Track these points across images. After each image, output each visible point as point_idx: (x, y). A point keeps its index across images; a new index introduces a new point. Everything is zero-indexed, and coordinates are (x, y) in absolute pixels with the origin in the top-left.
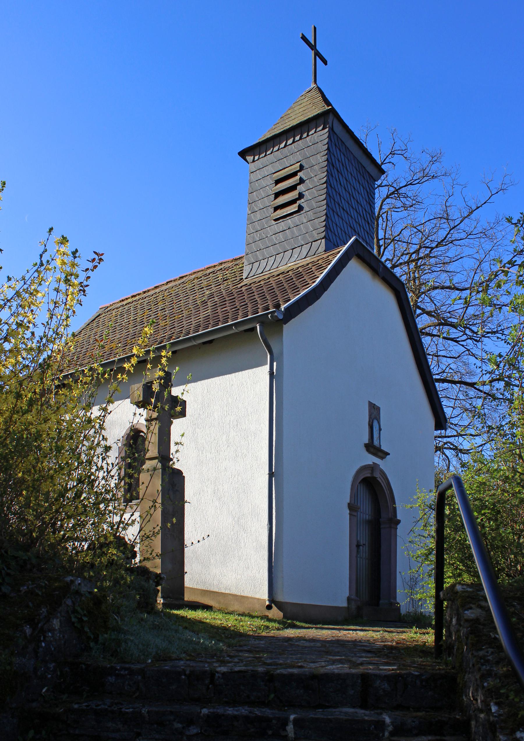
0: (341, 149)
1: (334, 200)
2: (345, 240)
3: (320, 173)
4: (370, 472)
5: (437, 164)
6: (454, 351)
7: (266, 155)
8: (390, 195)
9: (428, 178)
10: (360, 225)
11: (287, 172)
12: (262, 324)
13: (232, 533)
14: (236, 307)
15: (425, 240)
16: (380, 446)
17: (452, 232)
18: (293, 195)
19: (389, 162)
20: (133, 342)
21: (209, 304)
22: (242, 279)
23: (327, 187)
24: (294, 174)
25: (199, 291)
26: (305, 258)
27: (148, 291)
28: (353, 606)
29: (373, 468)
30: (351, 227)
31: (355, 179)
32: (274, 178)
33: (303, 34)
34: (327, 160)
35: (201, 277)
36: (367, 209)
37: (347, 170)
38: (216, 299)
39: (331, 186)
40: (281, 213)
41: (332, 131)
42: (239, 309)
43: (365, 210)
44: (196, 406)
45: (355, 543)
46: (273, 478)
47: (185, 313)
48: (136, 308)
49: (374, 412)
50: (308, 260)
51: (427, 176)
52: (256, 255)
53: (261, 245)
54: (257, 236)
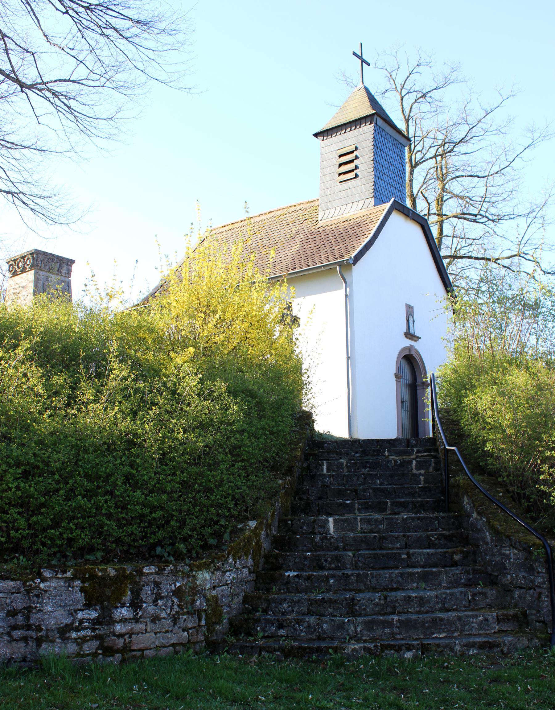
40: (343, 177)
49: (410, 310)
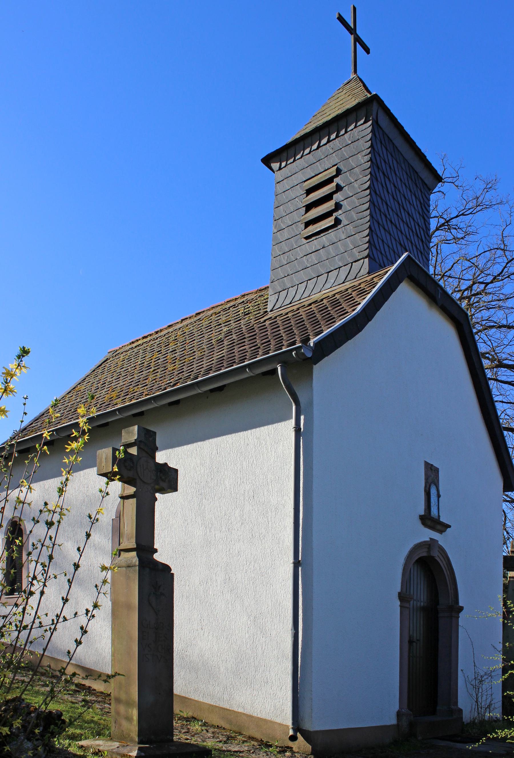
0: (388, 148)
1: (380, 211)
2: (394, 259)
3: (361, 176)
4: (426, 550)
5: (492, 192)
6: (511, 396)
7: (294, 161)
8: (440, 226)
9: (481, 207)
10: (412, 243)
11: (321, 178)
12: (285, 365)
13: (247, 636)
14: (257, 345)
15: (479, 275)
16: (439, 516)
17: (509, 265)
18: (329, 206)
19: (438, 191)
20: (135, 391)
21: (226, 343)
22: (267, 312)
23: (370, 194)
24: (330, 181)
25: (216, 328)
26: (343, 283)
27: (161, 331)
28: (405, 723)
29: (430, 545)
30: (401, 244)
31: (406, 186)
32: (305, 186)
33: (339, 14)
34: (371, 160)
35: (220, 313)
36: (420, 224)
37: (396, 174)
38: (234, 336)
39: (376, 193)
41: (376, 125)
42: (259, 348)
43: (418, 225)
44: (202, 471)
45: (406, 640)
46: (300, 568)
47: (198, 354)
48: (145, 350)
49: (432, 474)
50: (348, 285)
51: (480, 206)
52: (284, 283)
53: (288, 269)
54: (284, 258)
